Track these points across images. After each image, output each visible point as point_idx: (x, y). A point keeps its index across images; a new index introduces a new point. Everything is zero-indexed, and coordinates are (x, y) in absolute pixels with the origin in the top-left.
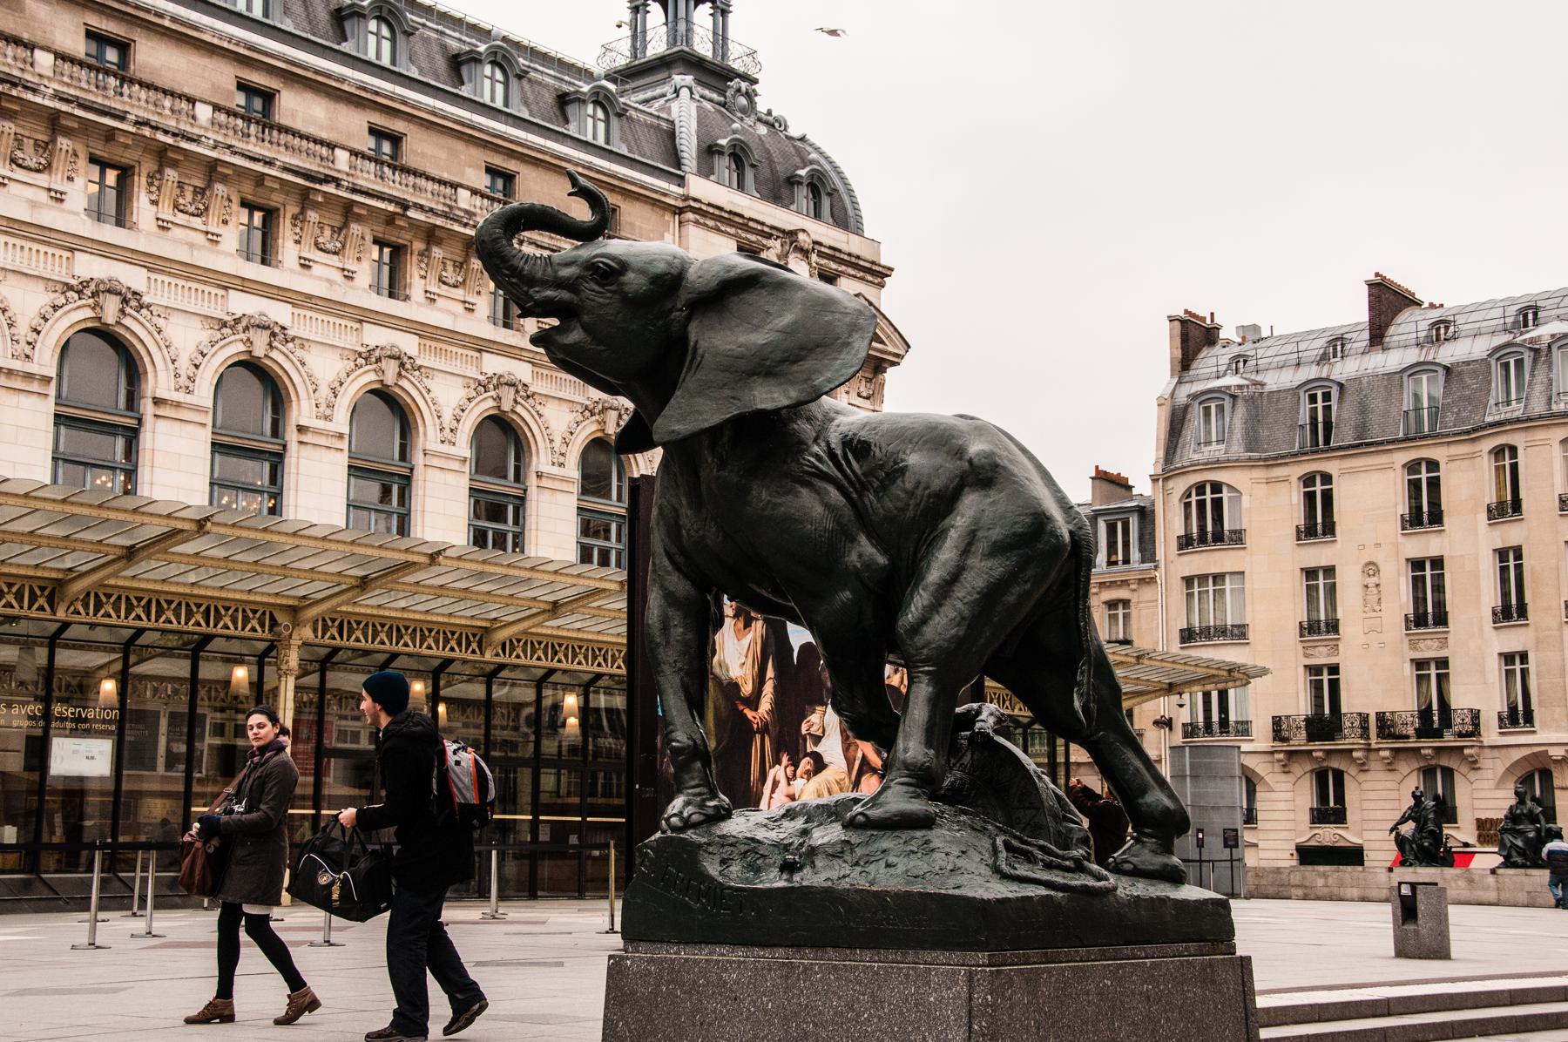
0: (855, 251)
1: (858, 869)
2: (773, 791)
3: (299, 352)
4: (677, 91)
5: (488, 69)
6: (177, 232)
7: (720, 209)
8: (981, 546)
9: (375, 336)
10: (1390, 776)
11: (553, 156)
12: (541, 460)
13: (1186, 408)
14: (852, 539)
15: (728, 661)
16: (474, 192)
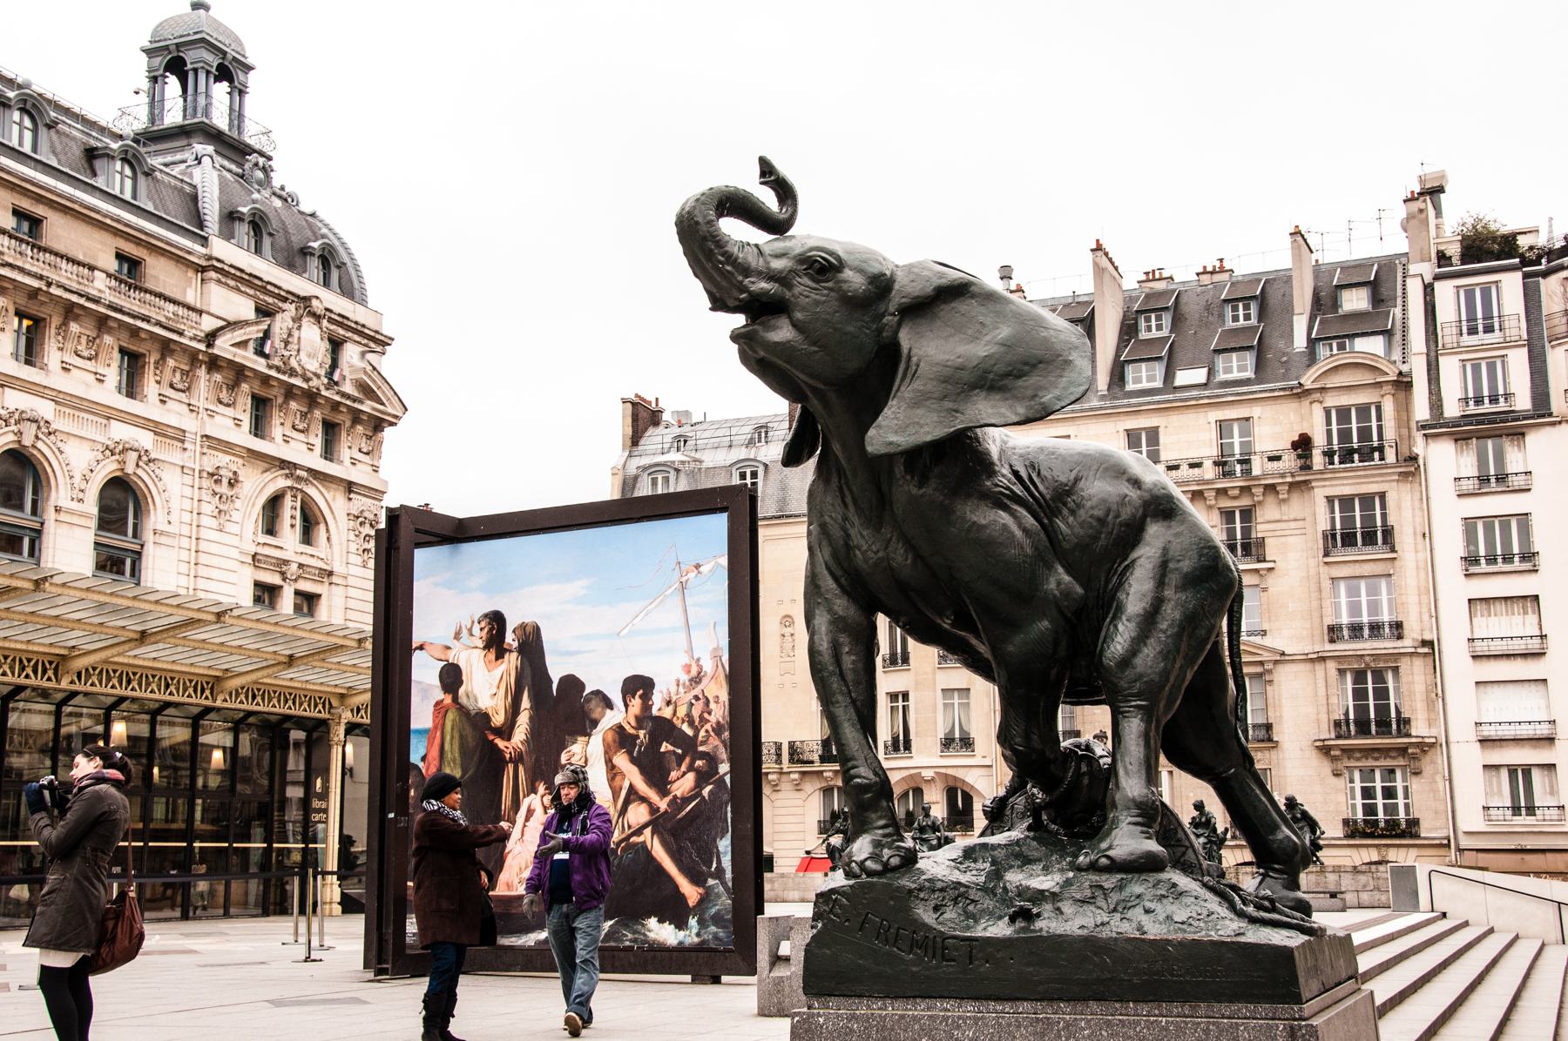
0: (362, 321)
1: (1118, 916)
2: (527, 819)
4: (199, 160)
5: (16, 115)
7: (242, 271)
8: (1173, 579)
10: (798, 795)
11: (82, 205)
12: (60, 495)
13: (636, 478)
14: (1050, 567)
15: (476, 691)
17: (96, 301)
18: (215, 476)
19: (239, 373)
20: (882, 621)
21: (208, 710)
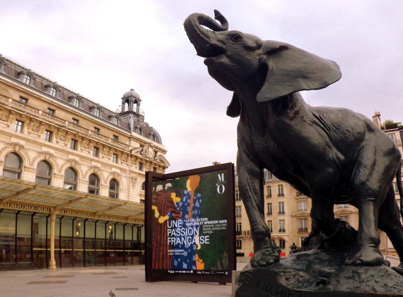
4: (130, 118)
6: (32, 134)
9: (94, 164)
12: (102, 182)
16: (92, 131)
17: (109, 144)
18: (132, 178)
19: (137, 157)
20: (265, 170)
21: (126, 224)
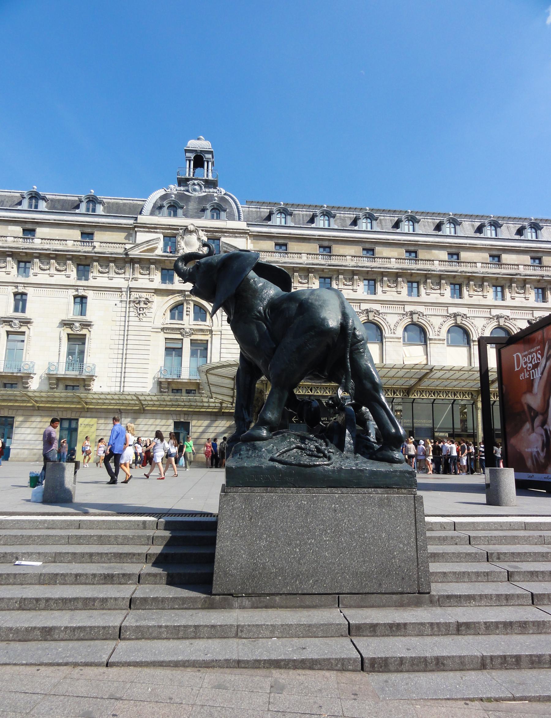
3: (514, 322)
9: (495, 312)
